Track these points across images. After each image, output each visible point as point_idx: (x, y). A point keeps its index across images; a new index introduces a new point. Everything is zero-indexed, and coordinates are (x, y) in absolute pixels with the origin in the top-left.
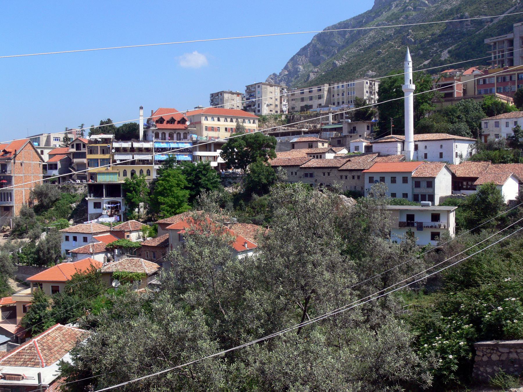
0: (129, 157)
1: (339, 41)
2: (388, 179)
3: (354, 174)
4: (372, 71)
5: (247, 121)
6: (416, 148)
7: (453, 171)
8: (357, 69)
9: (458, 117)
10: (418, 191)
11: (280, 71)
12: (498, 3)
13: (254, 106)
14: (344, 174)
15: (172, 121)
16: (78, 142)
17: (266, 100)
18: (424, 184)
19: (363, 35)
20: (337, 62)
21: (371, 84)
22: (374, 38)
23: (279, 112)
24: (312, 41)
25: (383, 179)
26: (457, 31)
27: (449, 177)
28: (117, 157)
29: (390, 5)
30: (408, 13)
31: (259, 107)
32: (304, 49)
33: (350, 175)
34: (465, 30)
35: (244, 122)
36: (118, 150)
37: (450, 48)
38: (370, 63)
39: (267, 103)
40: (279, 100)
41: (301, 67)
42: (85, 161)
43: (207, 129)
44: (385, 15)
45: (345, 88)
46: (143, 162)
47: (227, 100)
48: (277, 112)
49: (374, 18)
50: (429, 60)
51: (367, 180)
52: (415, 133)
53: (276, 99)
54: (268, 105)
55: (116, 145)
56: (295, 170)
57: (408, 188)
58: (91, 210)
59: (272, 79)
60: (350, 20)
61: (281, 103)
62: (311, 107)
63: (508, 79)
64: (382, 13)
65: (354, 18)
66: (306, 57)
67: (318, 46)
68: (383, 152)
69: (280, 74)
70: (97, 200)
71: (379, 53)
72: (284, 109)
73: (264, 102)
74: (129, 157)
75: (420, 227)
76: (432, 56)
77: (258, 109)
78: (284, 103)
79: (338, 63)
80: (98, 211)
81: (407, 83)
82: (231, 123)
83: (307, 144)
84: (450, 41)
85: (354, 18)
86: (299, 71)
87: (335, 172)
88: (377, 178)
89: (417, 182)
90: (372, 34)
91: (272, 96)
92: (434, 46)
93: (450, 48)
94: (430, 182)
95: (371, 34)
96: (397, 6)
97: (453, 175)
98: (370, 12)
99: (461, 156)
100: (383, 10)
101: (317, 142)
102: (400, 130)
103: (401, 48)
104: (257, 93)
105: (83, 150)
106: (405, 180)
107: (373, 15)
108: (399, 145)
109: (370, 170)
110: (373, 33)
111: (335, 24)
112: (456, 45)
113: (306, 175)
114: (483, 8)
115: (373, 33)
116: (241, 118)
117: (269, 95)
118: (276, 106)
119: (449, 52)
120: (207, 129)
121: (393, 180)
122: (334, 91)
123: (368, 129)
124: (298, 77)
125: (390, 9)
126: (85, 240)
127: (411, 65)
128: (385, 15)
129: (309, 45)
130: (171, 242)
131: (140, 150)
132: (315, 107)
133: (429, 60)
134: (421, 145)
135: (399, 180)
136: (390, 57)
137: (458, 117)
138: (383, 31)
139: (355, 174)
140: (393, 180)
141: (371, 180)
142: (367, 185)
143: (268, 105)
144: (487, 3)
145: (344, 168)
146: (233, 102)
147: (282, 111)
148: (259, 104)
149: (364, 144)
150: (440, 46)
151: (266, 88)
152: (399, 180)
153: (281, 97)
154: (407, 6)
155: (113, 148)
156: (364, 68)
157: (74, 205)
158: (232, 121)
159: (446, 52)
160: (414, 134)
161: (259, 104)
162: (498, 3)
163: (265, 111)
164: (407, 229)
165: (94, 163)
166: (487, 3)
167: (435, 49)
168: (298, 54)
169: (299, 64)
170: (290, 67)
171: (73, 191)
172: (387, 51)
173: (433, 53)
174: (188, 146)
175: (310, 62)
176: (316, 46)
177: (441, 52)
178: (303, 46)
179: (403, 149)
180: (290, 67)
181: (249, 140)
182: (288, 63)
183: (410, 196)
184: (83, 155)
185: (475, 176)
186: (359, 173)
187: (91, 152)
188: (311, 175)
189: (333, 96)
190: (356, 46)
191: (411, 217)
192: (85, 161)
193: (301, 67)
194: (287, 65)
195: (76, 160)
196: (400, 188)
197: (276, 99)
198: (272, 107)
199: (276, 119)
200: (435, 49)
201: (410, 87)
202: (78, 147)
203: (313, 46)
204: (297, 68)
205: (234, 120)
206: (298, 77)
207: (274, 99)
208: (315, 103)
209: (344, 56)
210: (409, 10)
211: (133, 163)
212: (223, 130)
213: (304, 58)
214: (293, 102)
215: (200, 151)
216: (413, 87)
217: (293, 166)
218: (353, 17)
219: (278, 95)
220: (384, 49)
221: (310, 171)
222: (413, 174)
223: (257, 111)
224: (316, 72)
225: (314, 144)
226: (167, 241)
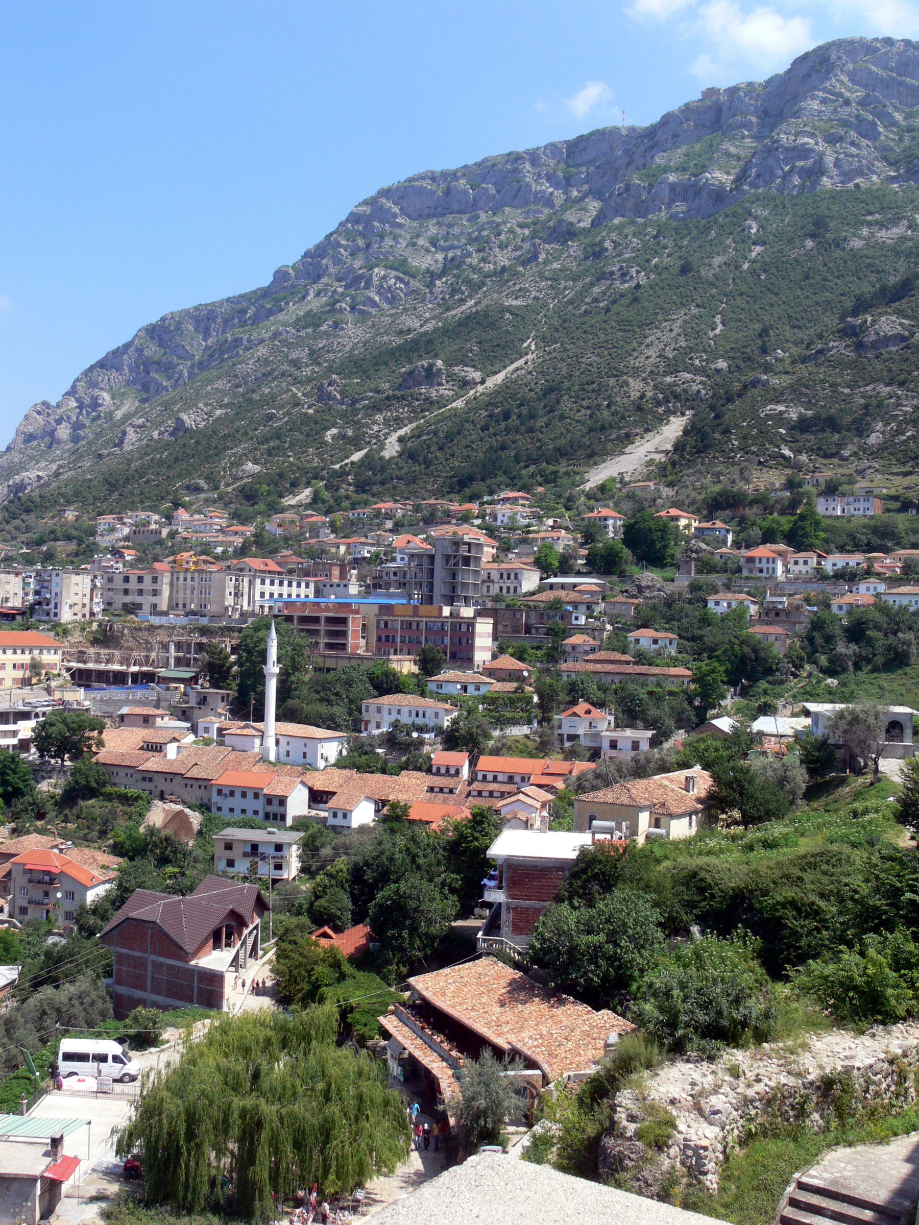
1: (196, 346)
2: (238, 794)
4: (256, 462)
5: (45, 652)
6: (277, 742)
7: (310, 784)
8: (225, 449)
9: (336, 694)
10: (269, 809)
12: (498, 345)
13: (48, 604)
14: (189, 782)
17: (69, 598)
18: (276, 802)
21: (237, 580)
22: (267, 362)
25: (232, 793)
27: (306, 792)
30: (338, 316)
31: (56, 608)
32: (117, 354)
33: (196, 784)
35: (41, 652)
37: (402, 432)
38: (251, 439)
39: (70, 602)
40: (88, 596)
44: (294, 310)
45: (196, 583)
48: (84, 616)
50: (365, 451)
51: (215, 792)
52: (278, 719)
54: (71, 606)
56: (130, 771)
57: (259, 805)
59: (39, 413)
60: (221, 303)
61: (91, 599)
62: (139, 606)
63: (414, 626)
64: (287, 304)
65: (228, 300)
68: (237, 747)
69: (58, 406)
71: (270, 417)
72: (96, 609)
73: (64, 600)
75: (264, 858)
76: (369, 443)
77: (53, 610)
78: (96, 600)
79: (188, 419)
83: (142, 719)
84: (404, 412)
86: (100, 405)
87: (179, 778)
88: (226, 791)
89: (269, 800)
91: (78, 589)
92: (375, 423)
94: (282, 801)
96: (318, 294)
97: (311, 790)
99: (326, 760)
100: (289, 298)
101: (155, 716)
103: (316, 411)
104: (54, 584)
106: (256, 796)
108: (257, 741)
110: (264, 351)
111: (187, 307)
112: (414, 425)
113: (144, 779)
114: (471, 351)
115: (264, 351)
117: (74, 589)
118: (84, 605)
119: (401, 440)
121: (244, 795)
124: (99, 417)
125: (304, 297)
127: (275, 643)
128: (294, 310)
129: (127, 346)
133: (365, 451)
135: (250, 795)
136: (291, 430)
137: (336, 694)
139: (203, 784)
140: (244, 795)
141: (220, 792)
142: (215, 798)
144: (480, 343)
145: (189, 775)
146: (8, 587)
147: (92, 614)
148: (56, 604)
150: (386, 422)
152: (250, 795)
154: (338, 301)
156: (239, 450)
161: (56, 604)
162: (498, 345)
163: (66, 616)
164: (251, 859)
166: (480, 343)
167: (376, 428)
169: (102, 389)
172: (288, 413)
173: (371, 437)
176: (142, 351)
178: (113, 347)
181: (72, 725)
182: (77, 380)
183: (261, 814)
186: (206, 783)
188: (150, 780)
190: (227, 375)
191: (255, 847)
193: (106, 396)
194: (74, 386)
196: (251, 804)
199: (83, 629)
200: (376, 428)
201: (273, 669)
203: (136, 350)
207: (80, 595)
208: (147, 601)
209: (201, 405)
210: (341, 310)
212: (9, 667)
214: (110, 594)
218: (226, 297)
220: (282, 407)
221: (150, 775)
222: (265, 791)
224: (140, 427)
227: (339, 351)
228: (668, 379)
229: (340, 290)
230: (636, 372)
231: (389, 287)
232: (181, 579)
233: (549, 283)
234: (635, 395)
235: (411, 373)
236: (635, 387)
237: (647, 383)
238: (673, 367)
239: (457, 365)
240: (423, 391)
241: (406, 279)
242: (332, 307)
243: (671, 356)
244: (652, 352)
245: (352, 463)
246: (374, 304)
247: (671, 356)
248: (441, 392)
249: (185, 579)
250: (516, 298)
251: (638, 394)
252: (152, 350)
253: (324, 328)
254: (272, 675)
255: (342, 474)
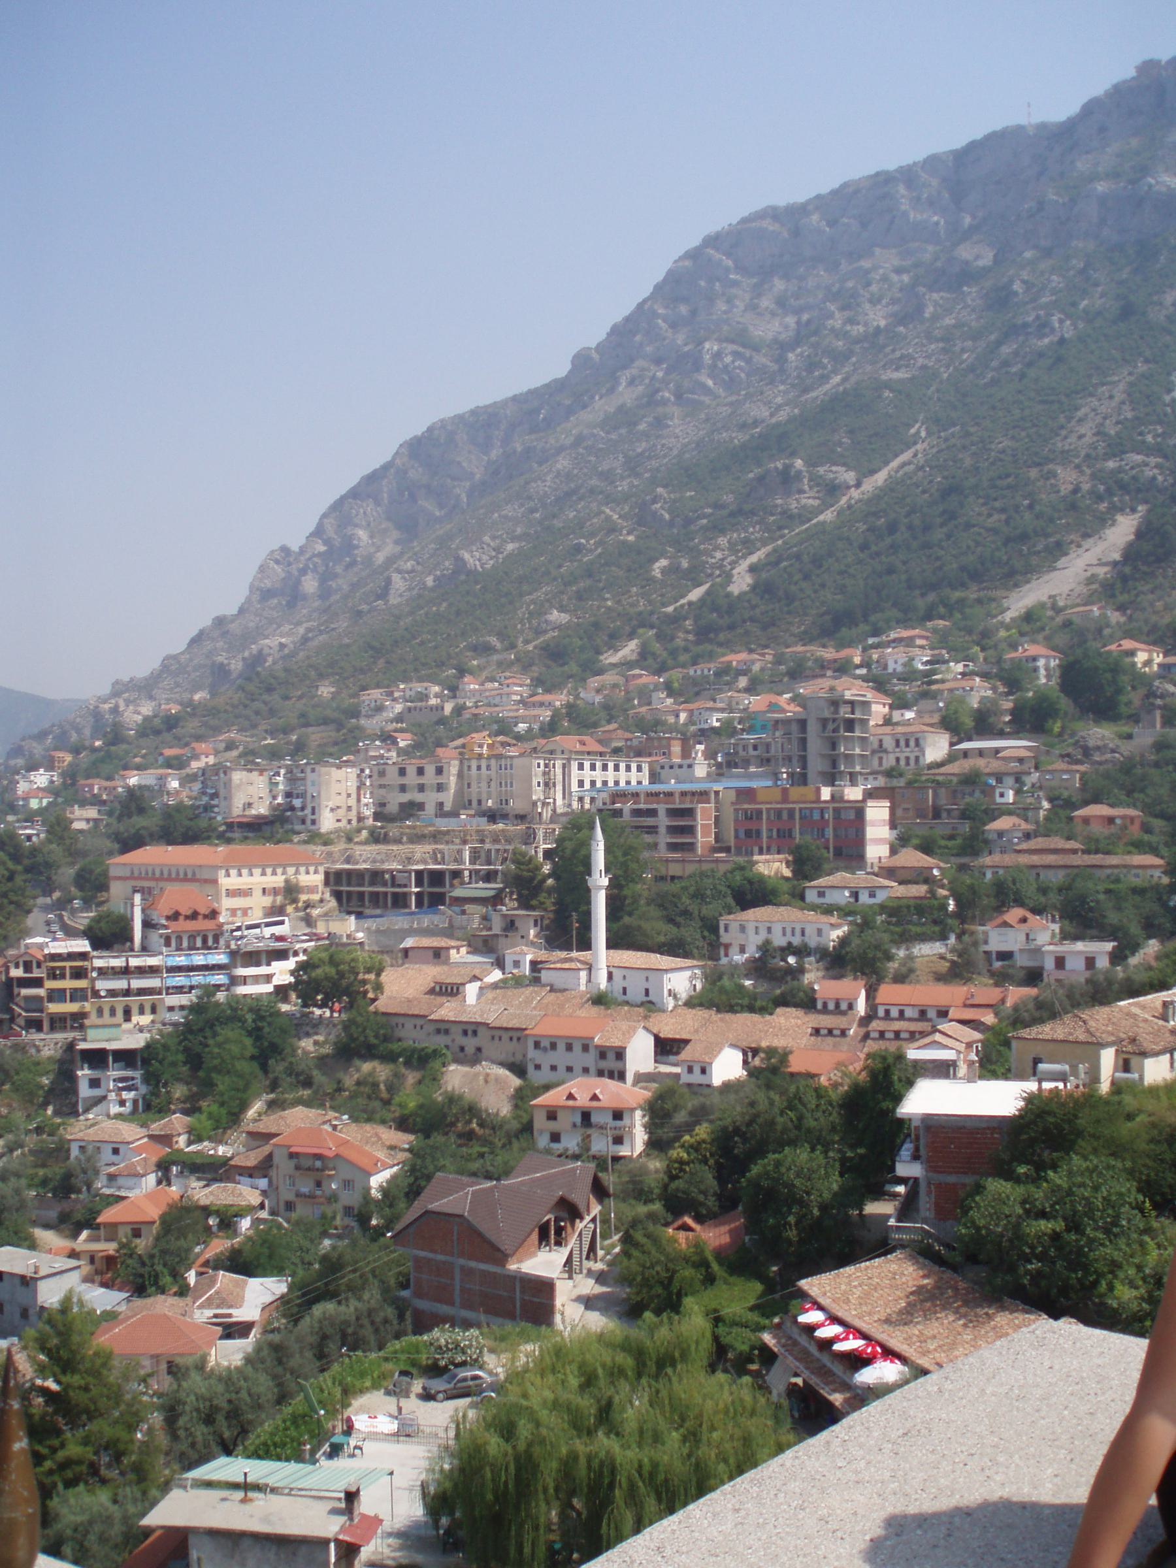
0: (121, 984)
1: (474, 464)
2: (561, 1046)
3: (511, 1033)
4: (562, 609)
5: (302, 869)
6: (610, 976)
8: (521, 595)
10: (603, 1064)
11: (303, 541)
14: (497, 1033)
15: (194, 916)
16: (27, 958)
18: (611, 1055)
19: (540, 464)
20: (467, 556)
21: (546, 766)
23: (354, 822)
24: (394, 458)
25: (553, 1046)
26: (776, 506)
27: (651, 1041)
28: (102, 985)
29: (616, 382)
30: (660, 410)
32: (372, 479)
33: (506, 1036)
34: (794, 505)
35: (297, 872)
36: (103, 972)
37: (754, 559)
39: (331, 804)
40: (354, 796)
41: (362, 534)
42: (41, 992)
43: (231, 893)
45: (493, 773)
46: (142, 992)
47: (239, 786)
48: (349, 821)
49: (570, 411)
51: (531, 1045)
52: (610, 946)
53: (349, 795)
54: (332, 810)
55: (98, 963)
58: (84, 1091)
59: (277, 562)
60: (505, 403)
61: (359, 800)
66: (378, 503)
67: (412, 474)
68: (559, 984)
69: (302, 550)
70: (95, 1074)
71: (578, 549)
74: (121, 984)
77: (310, 817)
78: (364, 801)
80: (97, 1092)
81: (596, 875)
82: (274, 878)
83: (431, 953)
85: (515, 399)
86: (357, 547)
88: (545, 1043)
89: (603, 1054)
90: (563, 463)
93: (754, 559)
95: (559, 466)
96: (632, 382)
98: (557, 387)
102: (585, 944)
103: (637, 537)
105: (36, 973)
106: (585, 1048)
107: (567, 402)
108: (583, 975)
109: (535, 1032)
110: (565, 463)
111: (460, 411)
113: (438, 1031)
114: (840, 444)
116: (291, 865)
117: (336, 788)
118: (349, 808)
120: (231, 893)
121: (569, 1048)
122: (469, 776)
123: (536, 925)
125: (612, 390)
126: (116, 1151)
127: (601, 846)
128: (602, 406)
129: (386, 467)
130: (276, 1159)
131: (142, 971)
132: (430, 809)
134: (617, 974)
135: (577, 1048)
138: (593, 459)
139: (515, 1035)
140: (569, 1048)
141: (537, 1045)
142: (532, 1053)
143: (332, 810)
148: (313, 809)
149: (529, 957)
151: (329, 774)
152: (577, 1048)
153: (359, 788)
154: (658, 391)
155: (93, 969)
156: (540, 594)
157: (45, 1081)
158: (274, 873)
159: (744, 565)
160: (608, 947)
161: (313, 809)
162: (876, 434)
165: (56, 996)
167: (719, 555)
168: (354, 494)
169: (356, 526)
170: (330, 531)
171: (33, 1051)
172: (601, 543)
173: (713, 566)
174: (221, 958)
175: (389, 519)
176: (405, 472)
177: (734, 564)
179: (589, 981)
180: (330, 531)
182: (324, 516)
183: (593, 1070)
184: (38, 983)
185: (684, 1036)
186: (519, 1034)
187: (53, 975)
188: (447, 1032)
189: (469, 785)
192: (41, 992)
193: (362, 534)
195: (25, 992)
196: (578, 1058)
197: (349, 795)
198: (341, 813)
200: (719, 555)
201: (600, 881)
202: (28, 967)
204: (351, 537)
205: (279, 871)
206: (353, 563)
207: (344, 795)
208: (430, 799)
209: (486, 539)
210: (664, 402)
211: (127, 992)
212: (257, 893)
213: (370, 506)
214: (383, 791)
215: (245, 966)
216: (605, 881)
217: (417, 1016)
218: (510, 394)
219: (352, 784)
220: (592, 535)
223: (308, 822)
225: (443, 953)
226: (270, 1157)
227: (665, 456)
228: (1111, 464)
229: (660, 374)
230: (1065, 457)
231: (726, 367)
232: (474, 767)
233: (941, 345)
234: (1065, 489)
235: (761, 479)
236: (1066, 477)
237: (1082, 472)
238: (1117, 449)
239: (822, 465)
240: (779, 501)
241: (748, 353)
242: (651, 400)
243: (1112, 432)
244: (1087, 429)
245: (690, 603)
246: (707, 391)
247: (1112, 432)
248: (804, 501)
249: (479, 768)
250: (897, 369)
251: (1070, 487)
252: (416, 474)
253: (642, 427)
254: (600, 888)
255: (676, 620)
